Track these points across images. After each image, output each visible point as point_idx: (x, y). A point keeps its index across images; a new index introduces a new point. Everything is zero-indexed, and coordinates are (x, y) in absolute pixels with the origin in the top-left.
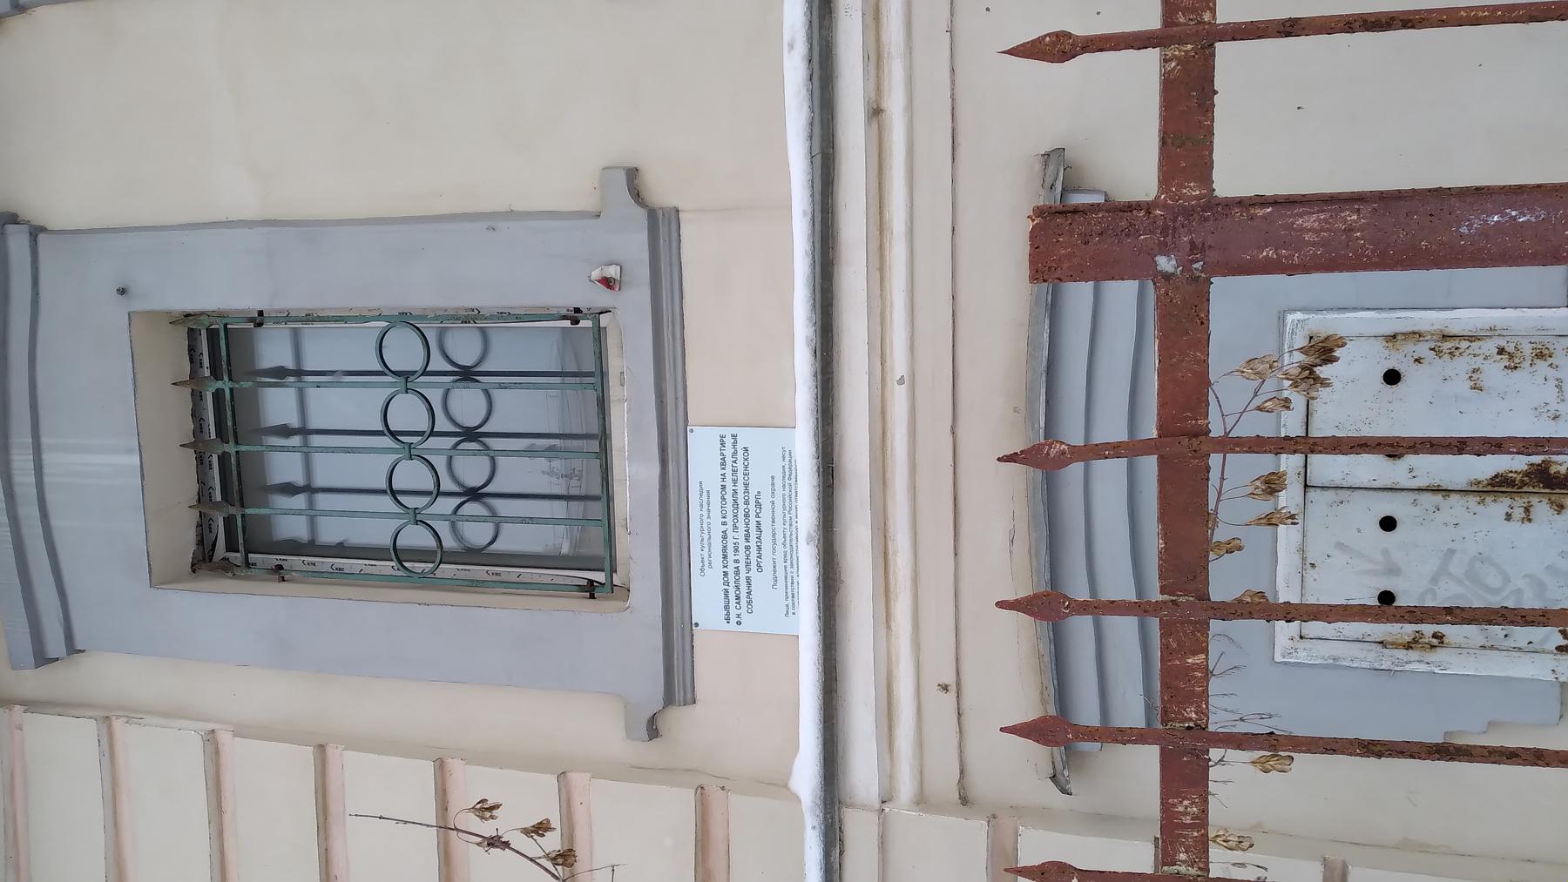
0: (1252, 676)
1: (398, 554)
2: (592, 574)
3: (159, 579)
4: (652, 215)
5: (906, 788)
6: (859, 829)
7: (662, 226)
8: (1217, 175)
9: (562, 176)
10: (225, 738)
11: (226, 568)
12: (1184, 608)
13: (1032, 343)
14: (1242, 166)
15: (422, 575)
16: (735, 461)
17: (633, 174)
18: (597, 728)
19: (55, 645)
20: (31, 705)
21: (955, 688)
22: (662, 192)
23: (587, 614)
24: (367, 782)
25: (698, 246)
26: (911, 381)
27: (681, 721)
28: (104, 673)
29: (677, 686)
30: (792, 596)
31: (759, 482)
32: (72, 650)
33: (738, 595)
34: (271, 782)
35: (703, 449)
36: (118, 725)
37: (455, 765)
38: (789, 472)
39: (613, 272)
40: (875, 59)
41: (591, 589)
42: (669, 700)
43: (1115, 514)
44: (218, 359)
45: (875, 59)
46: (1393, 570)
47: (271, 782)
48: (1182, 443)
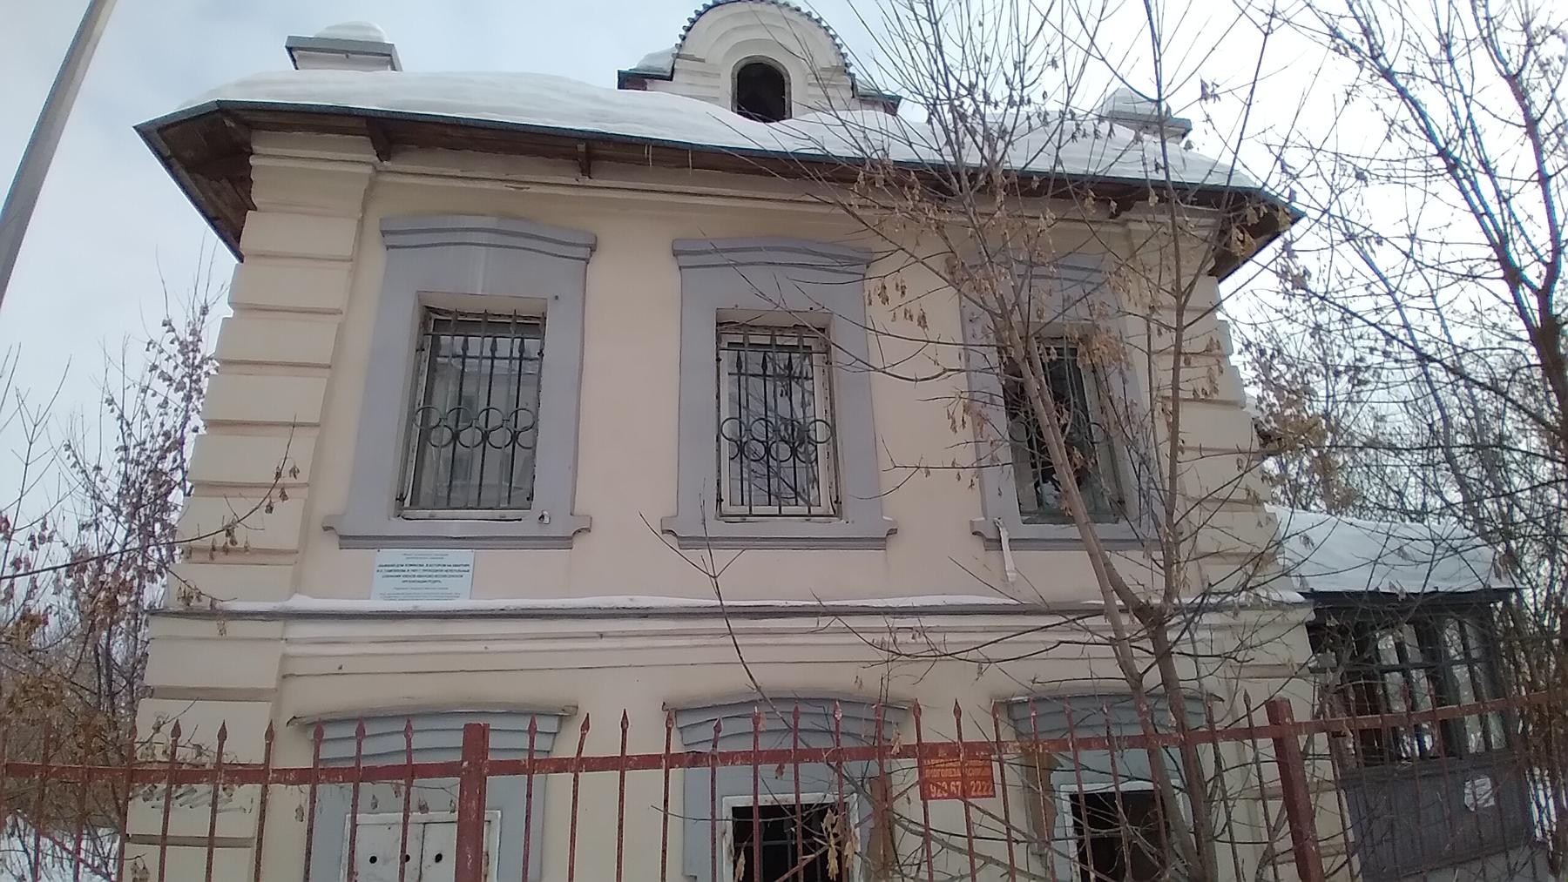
0: (333, 796)
1: (426, 410)
2: (408, 500)
3: (420, 295)
4: (570, 538)
5: (292, 650)
6: (273, 629)
7: (566, 542)
8: (327, 786)
9: (587, 501)
10: (338, 318)
11: (424, 324)
12: (358, 774)
13: (498, 704)
14: (496, 785)
15: (414, 420)
16: (461, 569)
17: (588, 530)
18: (332, 498)
19: (392, 240)
20: (361, 223)
21: (340, 673)
22: (579, 542)
23: (387, 501)
24: (302, 450)
25: (555, 557)
26: (486, 652)
27: (331, 542)
28: (376, 260)
29: (349, 541)
30: (390, 597)
31: (445, 582)
32: (388, 248)
33: (392, 571)
34: (314, 340)
35: (464, 556)
36: (348, 265)
37: (316, 431)
38: (450, 597)
39: (546, 520)
40: (623, 635)
41: (401, 499)
42: (341, 537)
43: (385, 746)
44: (532, 325)
45: (623, 635)
46: (386, 861)
47: (314, 340)
48: (410, 772)
